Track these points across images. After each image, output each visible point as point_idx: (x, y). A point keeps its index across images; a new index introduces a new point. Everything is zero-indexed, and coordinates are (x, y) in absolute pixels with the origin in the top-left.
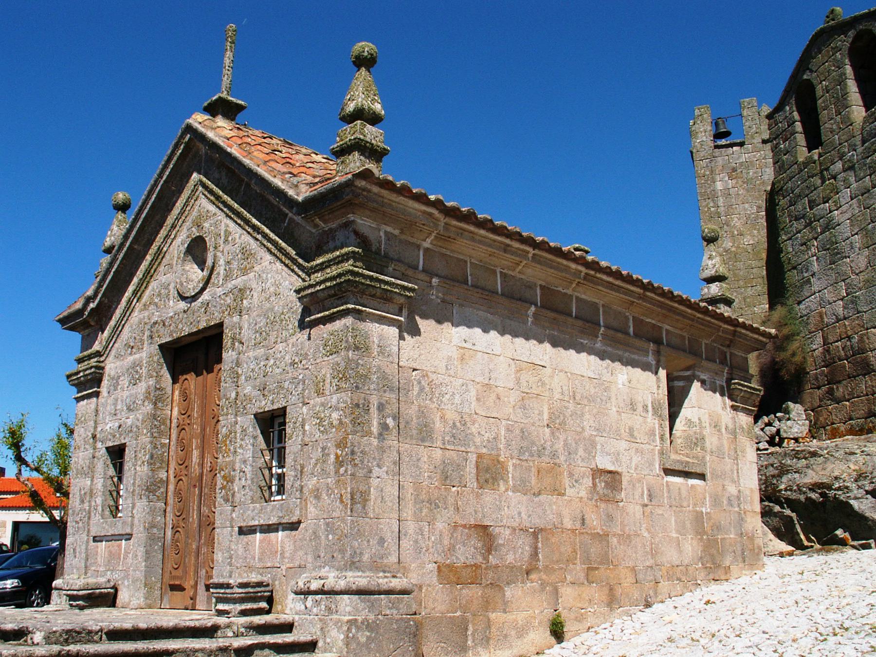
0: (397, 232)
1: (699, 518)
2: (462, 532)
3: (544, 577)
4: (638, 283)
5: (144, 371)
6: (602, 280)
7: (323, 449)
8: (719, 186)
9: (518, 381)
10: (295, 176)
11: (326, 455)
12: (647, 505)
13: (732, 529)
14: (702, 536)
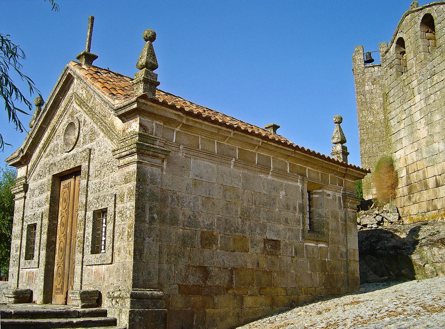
0: (162, 124)
1: (323, 263)
2: (192, 269)
3: (236, 292)
4: (291, 146)
5: (46, 187)
6: (271, 145)
7: (123, 228)
8: (367, 88)
9: (225, 196)
10: (115, 95)
11: (123, 232)
12: (294, 257)
13: (342, 270)
14: (325, 273)
